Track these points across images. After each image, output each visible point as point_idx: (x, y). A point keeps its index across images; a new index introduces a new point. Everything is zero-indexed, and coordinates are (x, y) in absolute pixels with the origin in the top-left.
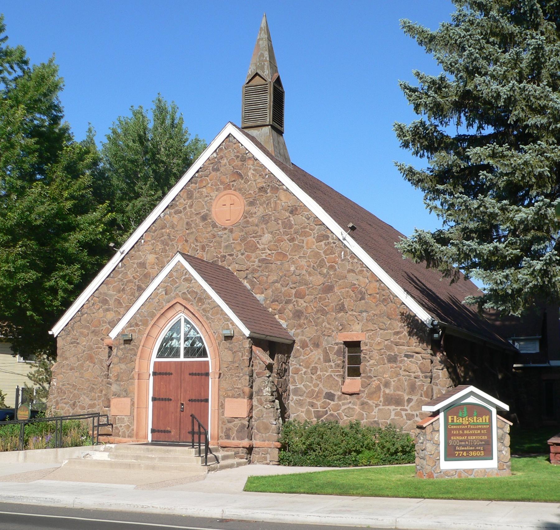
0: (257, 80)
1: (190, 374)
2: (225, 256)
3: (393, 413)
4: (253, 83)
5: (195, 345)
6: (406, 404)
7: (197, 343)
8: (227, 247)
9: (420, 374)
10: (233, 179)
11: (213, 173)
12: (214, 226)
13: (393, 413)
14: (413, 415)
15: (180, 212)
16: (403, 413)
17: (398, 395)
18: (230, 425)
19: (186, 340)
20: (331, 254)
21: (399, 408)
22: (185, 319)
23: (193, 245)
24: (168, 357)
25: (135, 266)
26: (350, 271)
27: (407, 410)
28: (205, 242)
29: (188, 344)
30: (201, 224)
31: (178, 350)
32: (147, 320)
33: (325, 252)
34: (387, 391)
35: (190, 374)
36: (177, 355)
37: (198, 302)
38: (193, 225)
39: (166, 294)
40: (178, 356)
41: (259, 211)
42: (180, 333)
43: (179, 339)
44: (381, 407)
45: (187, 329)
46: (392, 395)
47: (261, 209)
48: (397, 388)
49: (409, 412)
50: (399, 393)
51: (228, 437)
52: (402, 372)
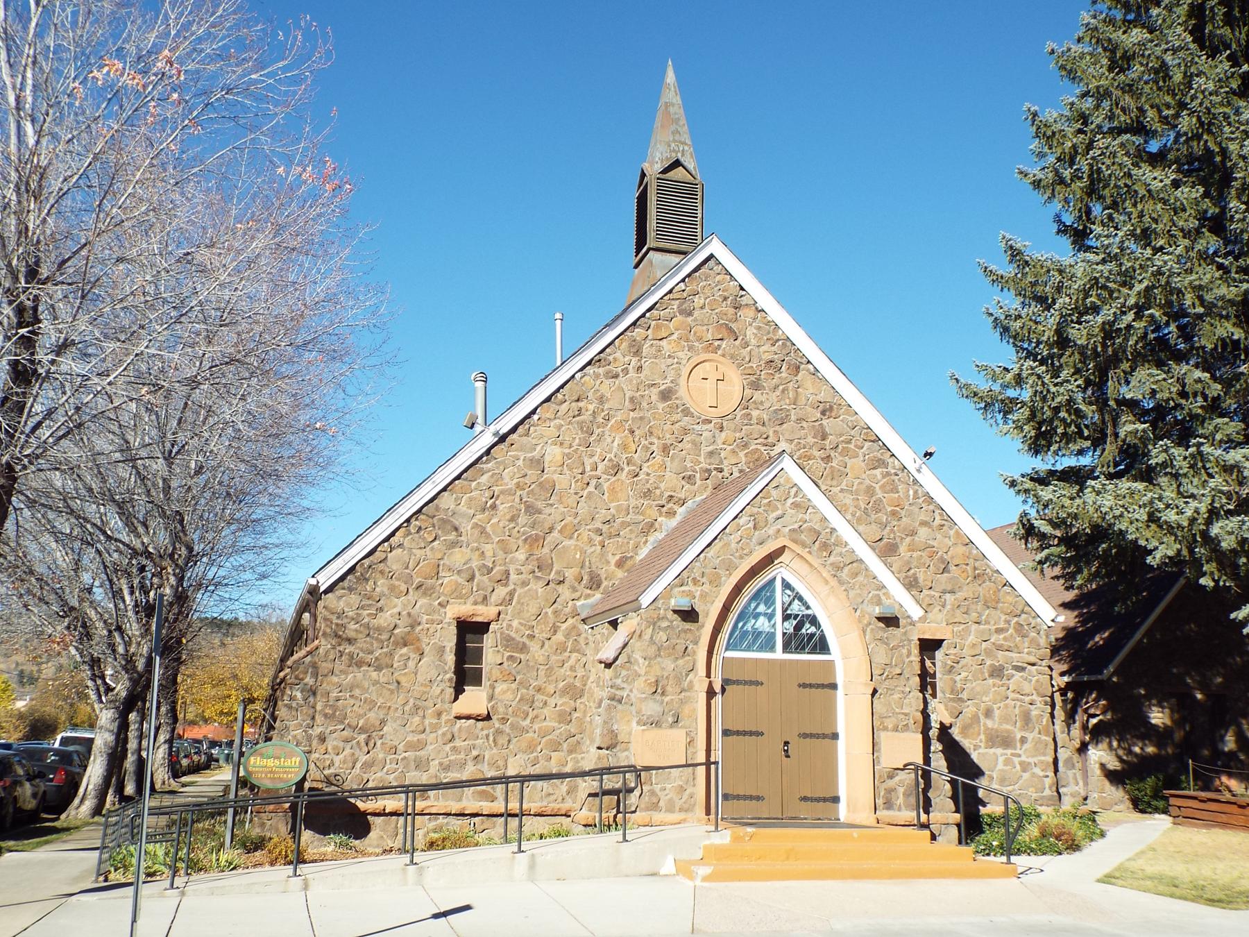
0: (679, 173)
1: (800, 686)
2: (709, 471)
3: (1001, 759)
4: (671, 175)
5: (803, 631)
6: (1018, 745)
7: (807, 625)
8: (711, 453)
9: (1034, 697)
10: (720, 336)
11: (680, 318)
12: (686, 412)
13: (1001, 759)
14: (1029, 764)
15: (616, 376)
16: (1016, 760)
17: (1008, 731)
18: (890, 783)
19: (786, 617)
20: (892, 491)
21: (1009, 752)
22: (783, 580)
23: (643, 442)
24: (748, 649)
25: (520, 463)
26: (924, 523)
27: (1020, 756)
28: (669, 439)
29: (790, 626)
30: (661, 406)
31: (771, 636)
32: (719, 576)
33: (882, 487)
34: (990, 723)
35: (800, 686)
36: (769, 645)
37: (820, 549)
38: (644, 404)
39: (755, 528)
40: (772, 648)
41: (769, 399)
42: (774, 603)
43: (770, 617)
44: (981, 751)
45: (787, 600)
46: (997, 731)
47: (774, 396)
48: (1005, 719)
49: (1023, 758)
50: (1009, 727)
51: (889, 805)
52: (1012, 695)
